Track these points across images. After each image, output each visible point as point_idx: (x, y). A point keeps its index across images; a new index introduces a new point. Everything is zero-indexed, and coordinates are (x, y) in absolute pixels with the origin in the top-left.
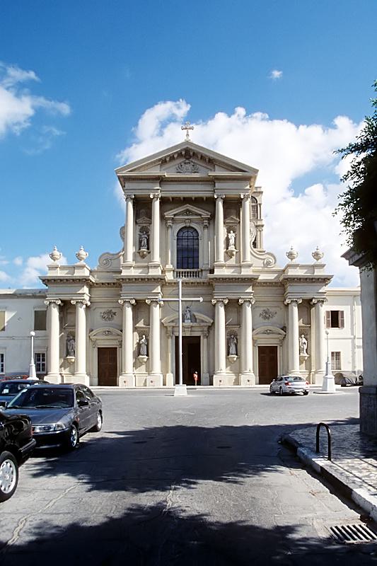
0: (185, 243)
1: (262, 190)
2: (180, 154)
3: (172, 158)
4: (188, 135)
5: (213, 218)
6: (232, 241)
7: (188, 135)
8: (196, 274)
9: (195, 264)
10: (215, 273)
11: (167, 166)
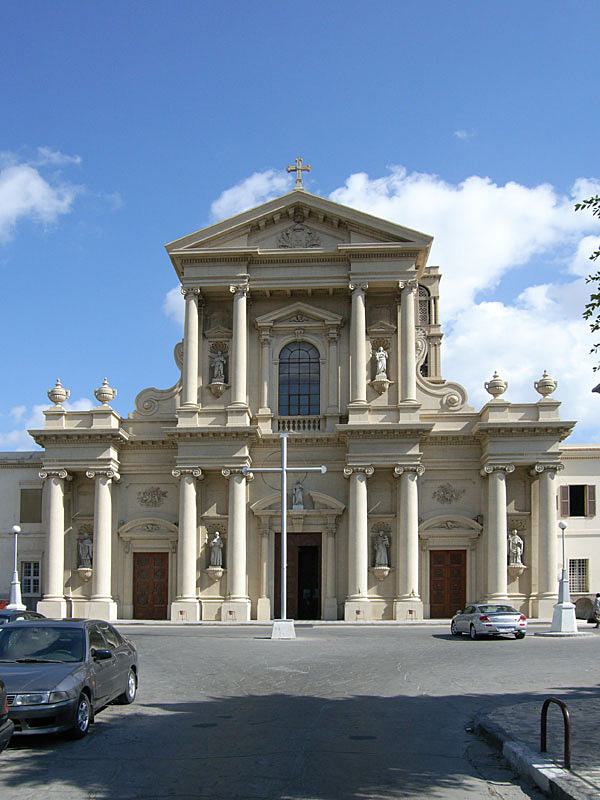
1: (440, 272)
2: (284, 215)
3: (270, 222)
5: (347, 324)
6: (382, 365)
8: (316, 425)
9: (313, 406)
10: (349, 423)
11: (260, 235)
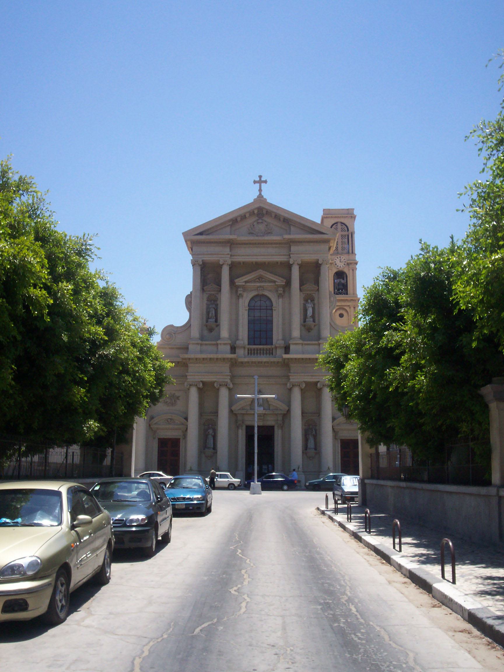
0: (257, 314)
4: (260, 190)
7: (260, 190)
9: (269, 340)
